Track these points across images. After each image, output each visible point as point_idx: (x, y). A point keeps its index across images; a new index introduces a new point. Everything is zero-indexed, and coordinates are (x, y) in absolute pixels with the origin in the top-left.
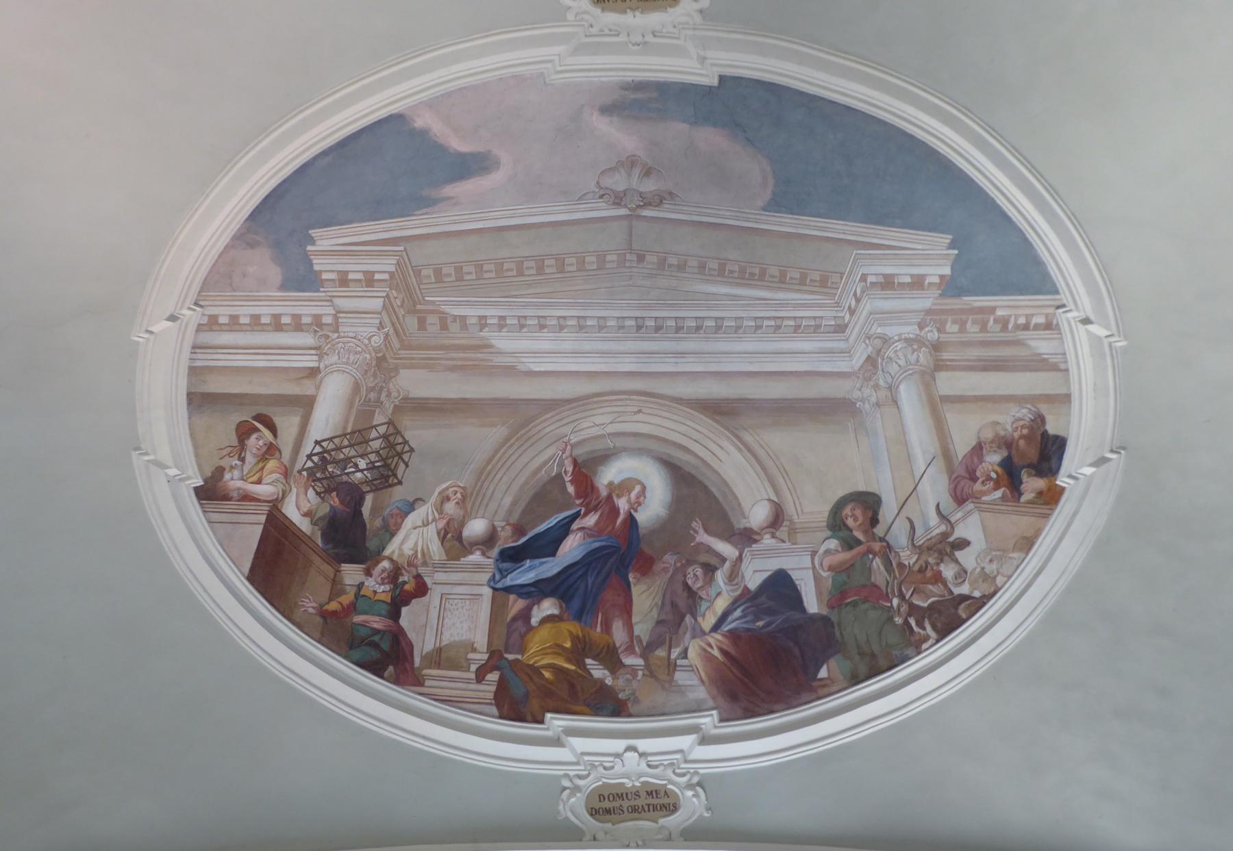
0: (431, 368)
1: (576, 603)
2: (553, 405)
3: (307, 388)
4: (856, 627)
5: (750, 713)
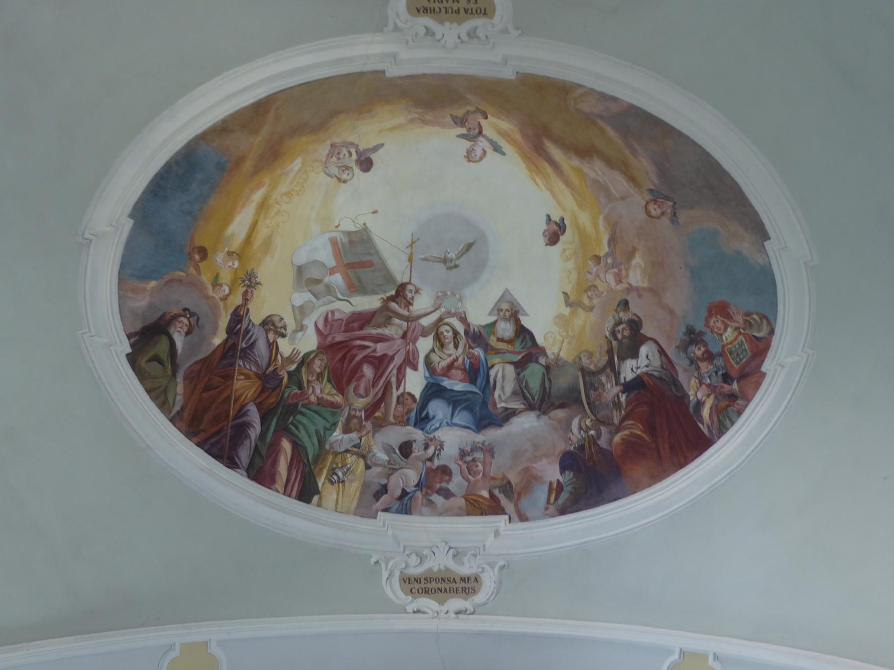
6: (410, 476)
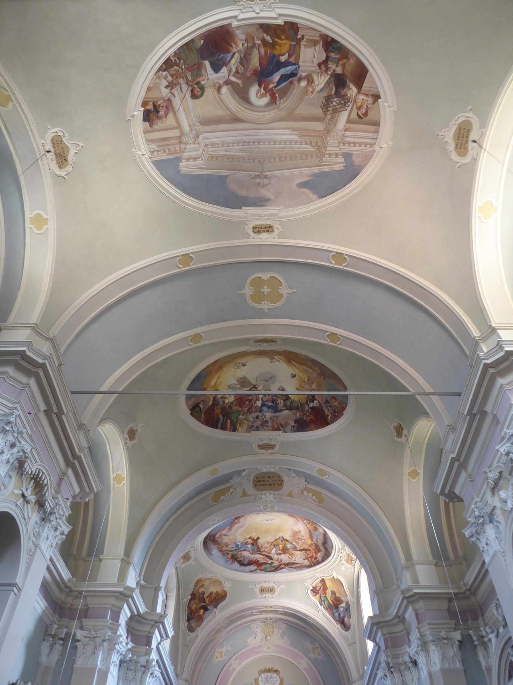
0: (315, 130)
1: (275, 60)
2: (282, 120)
3: (348, 126)
4: (194, 57)
5: (222, 27)
6: (259, 423)
